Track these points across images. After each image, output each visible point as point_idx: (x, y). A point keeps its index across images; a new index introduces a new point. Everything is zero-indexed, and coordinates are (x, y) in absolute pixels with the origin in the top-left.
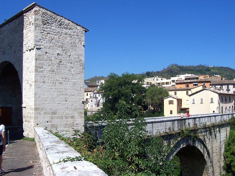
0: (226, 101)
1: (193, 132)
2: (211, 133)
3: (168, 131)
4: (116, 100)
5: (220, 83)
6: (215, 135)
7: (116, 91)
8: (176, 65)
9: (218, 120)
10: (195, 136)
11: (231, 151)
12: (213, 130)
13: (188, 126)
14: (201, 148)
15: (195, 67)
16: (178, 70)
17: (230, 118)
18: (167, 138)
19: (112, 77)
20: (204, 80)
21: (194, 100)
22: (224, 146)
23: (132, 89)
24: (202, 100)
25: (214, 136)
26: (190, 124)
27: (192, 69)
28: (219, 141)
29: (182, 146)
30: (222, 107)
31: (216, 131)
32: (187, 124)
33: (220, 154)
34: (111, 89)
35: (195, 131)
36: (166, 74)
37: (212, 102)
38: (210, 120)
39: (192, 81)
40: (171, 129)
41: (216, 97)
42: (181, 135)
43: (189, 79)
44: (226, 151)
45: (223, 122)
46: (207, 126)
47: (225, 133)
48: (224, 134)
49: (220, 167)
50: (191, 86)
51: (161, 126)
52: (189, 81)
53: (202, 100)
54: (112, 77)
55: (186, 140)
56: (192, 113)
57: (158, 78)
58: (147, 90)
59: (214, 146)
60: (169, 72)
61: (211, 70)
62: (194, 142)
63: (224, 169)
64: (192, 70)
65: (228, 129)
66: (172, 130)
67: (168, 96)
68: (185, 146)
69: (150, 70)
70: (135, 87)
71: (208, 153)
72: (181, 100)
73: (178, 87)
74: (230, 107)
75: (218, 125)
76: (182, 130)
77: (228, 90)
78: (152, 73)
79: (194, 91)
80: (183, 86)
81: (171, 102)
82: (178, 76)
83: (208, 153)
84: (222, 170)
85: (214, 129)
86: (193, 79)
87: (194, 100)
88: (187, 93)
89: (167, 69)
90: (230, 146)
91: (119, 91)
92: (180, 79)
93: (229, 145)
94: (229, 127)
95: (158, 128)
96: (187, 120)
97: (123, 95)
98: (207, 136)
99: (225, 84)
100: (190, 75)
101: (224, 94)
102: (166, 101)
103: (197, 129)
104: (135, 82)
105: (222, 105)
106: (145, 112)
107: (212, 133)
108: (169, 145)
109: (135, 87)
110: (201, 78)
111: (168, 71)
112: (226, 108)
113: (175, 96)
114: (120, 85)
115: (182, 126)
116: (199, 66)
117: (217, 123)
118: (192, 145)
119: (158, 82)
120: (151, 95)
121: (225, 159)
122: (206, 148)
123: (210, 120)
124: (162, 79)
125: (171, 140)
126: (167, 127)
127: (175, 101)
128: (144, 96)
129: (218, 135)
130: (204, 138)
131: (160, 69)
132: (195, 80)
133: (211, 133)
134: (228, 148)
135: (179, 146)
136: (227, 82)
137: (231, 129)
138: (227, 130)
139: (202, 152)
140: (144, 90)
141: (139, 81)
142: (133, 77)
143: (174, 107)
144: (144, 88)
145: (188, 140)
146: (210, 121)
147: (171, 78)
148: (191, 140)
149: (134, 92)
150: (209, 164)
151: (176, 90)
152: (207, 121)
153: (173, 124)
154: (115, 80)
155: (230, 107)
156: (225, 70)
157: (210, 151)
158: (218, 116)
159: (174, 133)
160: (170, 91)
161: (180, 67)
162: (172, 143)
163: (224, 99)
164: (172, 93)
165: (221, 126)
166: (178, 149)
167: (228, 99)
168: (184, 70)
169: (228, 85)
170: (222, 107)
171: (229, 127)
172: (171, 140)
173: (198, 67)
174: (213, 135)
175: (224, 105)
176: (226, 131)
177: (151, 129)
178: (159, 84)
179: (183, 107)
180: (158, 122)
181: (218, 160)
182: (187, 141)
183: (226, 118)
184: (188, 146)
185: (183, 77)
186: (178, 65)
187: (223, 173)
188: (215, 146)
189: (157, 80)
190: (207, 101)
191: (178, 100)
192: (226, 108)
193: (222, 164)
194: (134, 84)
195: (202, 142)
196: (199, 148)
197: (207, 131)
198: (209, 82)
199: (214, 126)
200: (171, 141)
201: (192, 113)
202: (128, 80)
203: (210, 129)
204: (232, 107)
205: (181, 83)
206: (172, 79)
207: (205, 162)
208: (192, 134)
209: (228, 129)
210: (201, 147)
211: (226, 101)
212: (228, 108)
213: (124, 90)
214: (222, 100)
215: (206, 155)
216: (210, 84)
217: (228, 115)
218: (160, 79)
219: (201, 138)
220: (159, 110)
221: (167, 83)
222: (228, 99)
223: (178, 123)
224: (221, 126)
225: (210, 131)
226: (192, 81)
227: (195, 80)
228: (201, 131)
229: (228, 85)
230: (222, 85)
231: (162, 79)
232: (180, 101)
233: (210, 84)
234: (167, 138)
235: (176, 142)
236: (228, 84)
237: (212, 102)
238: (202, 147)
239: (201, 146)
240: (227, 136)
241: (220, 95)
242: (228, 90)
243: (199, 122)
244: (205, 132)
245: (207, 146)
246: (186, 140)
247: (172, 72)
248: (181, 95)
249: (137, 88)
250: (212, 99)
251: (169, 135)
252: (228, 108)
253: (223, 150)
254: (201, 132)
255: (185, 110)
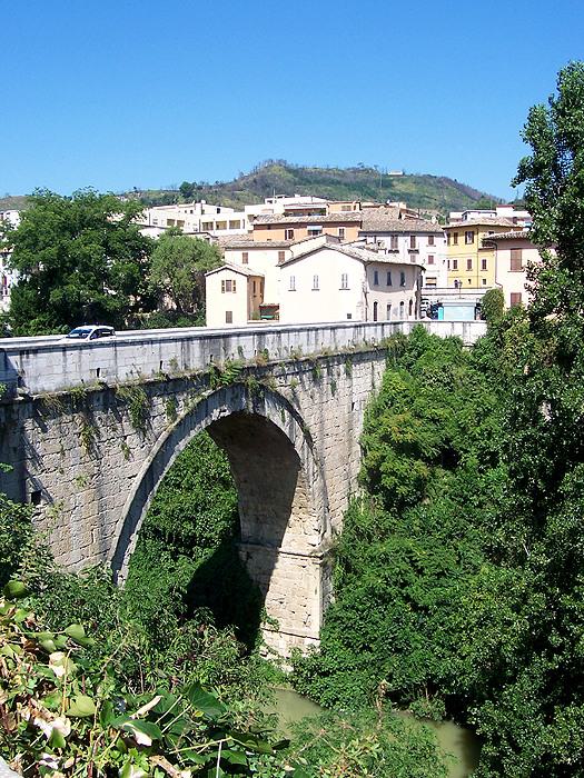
0: (389, 283)
1: (255, 373)
2: (316, 379)
3: (167, 369)
4: (52, 277)
5: (390, 230)
6: (334, 386)
7: (54, 250)
8: (280, 162)
9: (344, 340)
10: (262, 386)
11: (380, 431)
12: (326, 370)
13: (237, 355)
14: (284, 421)
15: (343, 174)
16: (289, 181)
17: (387, 335)
18: (165, 390)
19: (42, 201)
20: (343, 219)
21: (293, 280)
22: (362, 418)
23: (105, 244)
24: (316, 279)
25: (326, 387)
26: (276, 350)
27: (332, 177)
28: (345, 401)
29: (216, 415)
30: (376, 303)
31: (335, 373)
32: (234, 349)
33: (350, 441)
34: (36, 243)
35: (261, 370)
36: (246, 192)
37: (345, 288)
38: (317, 340)
39: (306, 218)
40: (179, 363)
41: (357, 273)
42: (212, 384)
43: (296, 213)
44: (369, 430)
45: (362, 348)
46: (303, 358)
47: (369, 380)
48: (365, 382)
49: (348, 476)
50: (300, 233)
51: (144, 354)
52: (295, 219)
53: (316, 279)
54: (40, 202)
55: (229, 395)
56: (287, 317)
57: (206, 207)
58: (156, 245)
59: (327, 415)
60: (259, 186)
61: (394, 183)
62: (258, 402)
63: (362, 482)
64: (324, 182)
65: (380, 366)
66: (182, 368)
67: (222, 266)
68: (227, 413)
69: (193, 178)
70: (114, 235)
71: (308, 436)
72: (263, 278)
73: (261, 237)
74: (402, 303)
75: (342, 355)
76: (215, 368)
77: (413, 251)
78: (200, 188)
79: (297, 250)
80: (278, 236)
81: (228, 286)
82: (271, 202)
83: (308, 436)
84: (355, 485)
85: (328, 367)
86: (309, 212)
87: (293, 280)
88: (282, 255)
89: (252, 175)
90: (381, 418)
91: (63, 250)
92: (270, 213)
93: (378, 412)
94: (384, 361)
95: (133, 361)
96: (234, 338)
97: (74, 262)
98: (304, 387)
99: (406, 233)
100: (307, 200)
101: (376, 262)
102: (213, 283)
103: (264, 364)
104: (117, 218)
105: (374, 295)
106: (148, 315)
107: (321, 377)
108: (172, 412)
109: (114, 235)
110: (335, 210)
111: (255, 181)
112: (389, 306)
113: (245, 265)
114: (68, 228)
115: (215, 354)
116: (355, 171)
117: (340, 348)
118: (251, 411)
119: (206, 219)
120: (167, 262)
121: (365, 454)
122: (300, 420)
123: (317, 340)
124: (218, 211)
125: (177, 397)
126: (166, 360)
127: (242, 284)
128: (144, 265)
129: (342, 383)
130: (294, 393)
131: (228, 176)
132: (315, 218)
133: (316, 379)
134: (373, 422)
135: (208, 414)
136: (411, 226)
137: (390, 366)
138: (376, 371)
139: (286, 431)
140: (141, 247)
141: (129, 217)
142: (111, 204)
143: (238, 303)
144: (145, 239)
145: (237, 397)
146: (316, 344)
147: (247, 207)
148: (247, 396)
149: (112, 253)
150: (309, 467)
151: (245, 249)
152: (305, 344)
153: (186, 352)
154: (50, 214)
155: (402, 303)
156: (438, 188)
157: (314, 430)
158: (345, 327)
159: (187, 375)
160: (227, 249)
161: (295, 172)
162: (182, 403)
163: (383, 278)
164: (233, 258)
165: (353, 358)
166: (203, 423)
167: (396, 279)
168: (310, 183)
169: (413, 235)
170: (376, 303)
171: (384, 361)
172: (177, 397)
173: (354, 172)
174: (325, 382)
175: (383, 298)
176: (373, 374)
177: (112, 362)
178: (208, 225)
179: (268, 301)
180: (133, 343)
181: (342, 458)
182: (235, 399)
183: (374, 336)
184: (238, 415)
185: (276, 207)
186: (289, 163)
187: (357, 495)
188: (330, 416)
189: (203, 212)
190: (330, 283)
191: (249, 277)
192: (389, 306)
193: (357, 468)
194: (112, 227)
195: (287, 405)
196: (277, 420)
197: (304, 372)
198: (359, 224)
199: (328, 359)
200: (180, 398)
201: (287, 317)
202: (90, 212)
203: (312, 367)
204: (411, 302)
205: (269, 227)
206: (251, 210)
207: (297, 463)
208: (251, 380)
209: (380, 366)
210: (283, 417)
211: (389, 283)
212: (396, 305)
213: (84, 246)
214: (376, 282)
215: (299, 442)
216: (360, 233)
217: (380, 327)
218: (211, 209)
219: (285, 391)
220: (191, 306)
221: (234, 224)
222: (396, 279)
223: (202, 346)
224: (353, 358)
225: (314, 370)
226: (306, 218)
227: (315, 218)
228: (283, 370)
229: (413, 235)
230: (394, 235)
231: (218, 211)
232: (256, 284)
233: (360, 233)
234: (165, 390)
235: (197, 400)
236: (412, 232)
237: (345, 288)
238: (287, 419)
239: (283, 414)
240: (374, 387)
241: (367, 264)
242: (413, 251)
243: (276, 345)
244: (297, 373)
245: (304, 414)
246: (229, 395)
247: (267, 186)
248: (262, 263)
249: (123, 241)
250: (344, 278)
251: (169, 380)
252: (396, 305)
253: (359, 429)
254: (284, 375)
255: (271, 311)
